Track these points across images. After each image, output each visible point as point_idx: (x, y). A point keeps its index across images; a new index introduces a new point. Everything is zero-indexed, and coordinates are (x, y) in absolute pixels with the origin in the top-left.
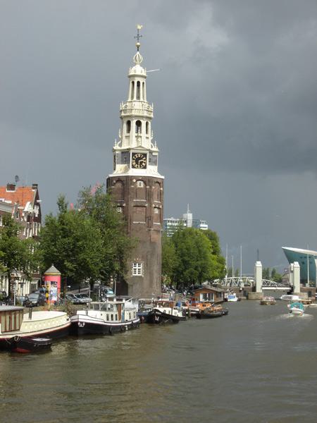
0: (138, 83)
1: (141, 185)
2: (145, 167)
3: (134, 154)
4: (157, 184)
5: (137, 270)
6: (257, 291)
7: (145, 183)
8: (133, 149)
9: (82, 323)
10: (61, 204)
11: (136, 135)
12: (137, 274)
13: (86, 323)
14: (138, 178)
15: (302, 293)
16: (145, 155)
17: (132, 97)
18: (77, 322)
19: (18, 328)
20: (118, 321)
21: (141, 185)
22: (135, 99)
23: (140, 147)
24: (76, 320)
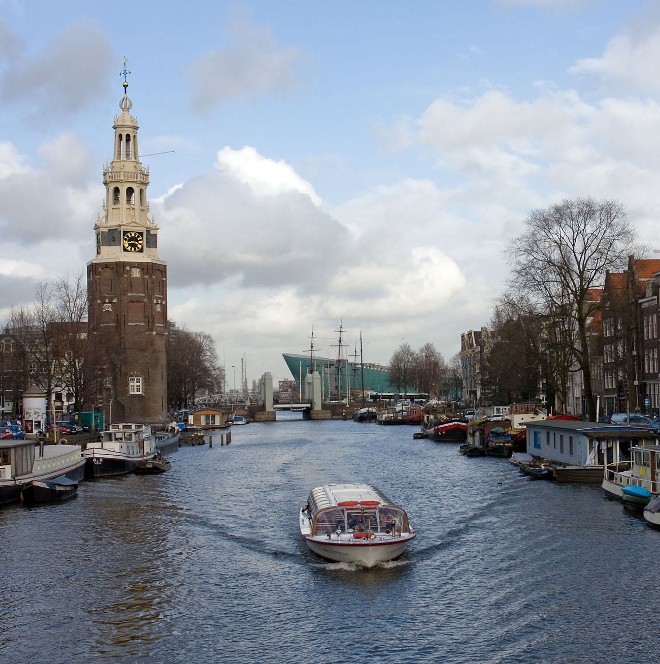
0: (128, 136)
1: (136, 273)
2: (141, 251)
3: (125, 233)
4: (158, 272)
5: (135, 387)
6: (267, 410)
7: (142, 269)
8: (124, 225)
9: (98, 459)
10: (639, 232)
11: (128, 206)
12: (136, 393)
13: (104, 459)
14: (133, 265)
15: (324, 411)
16: (141, 234)
17: (128, 155)
18: (92, 458)
19: (29, 470)
20: (135, 455)
21: (136, 273)
22: (123, 157)
23: (134, 222)
24: (92, 456)
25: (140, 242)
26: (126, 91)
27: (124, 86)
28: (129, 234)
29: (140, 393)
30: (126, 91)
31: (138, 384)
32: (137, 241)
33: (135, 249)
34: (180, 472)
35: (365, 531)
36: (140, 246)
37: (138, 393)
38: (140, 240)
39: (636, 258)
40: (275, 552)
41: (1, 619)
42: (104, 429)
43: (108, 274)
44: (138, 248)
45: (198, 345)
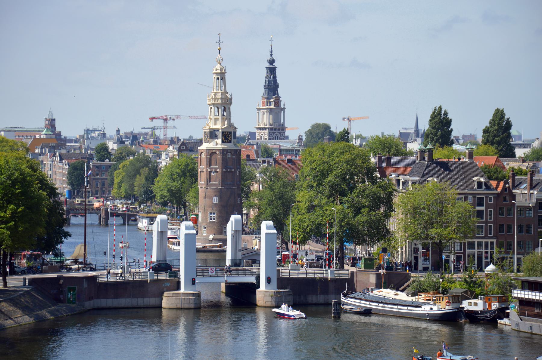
25: (227, 133)
26: (219, 52)
27: (218, 49)
28: (225, 133)
29: (215, 221)
30: (219, 52)
31: (214, 216)
32: (226, 135)
33: (228, 141)
34: (167, 353)
35: (349, 195)
36: (230, 139)
37: (214, 221)
38: (230, 136)
39: (67, 138)
40: (413, 281)
41: (1, 228)
42: (212, 218)
43: (229, 155)
44: (229, 140)
45: (231, 337)
